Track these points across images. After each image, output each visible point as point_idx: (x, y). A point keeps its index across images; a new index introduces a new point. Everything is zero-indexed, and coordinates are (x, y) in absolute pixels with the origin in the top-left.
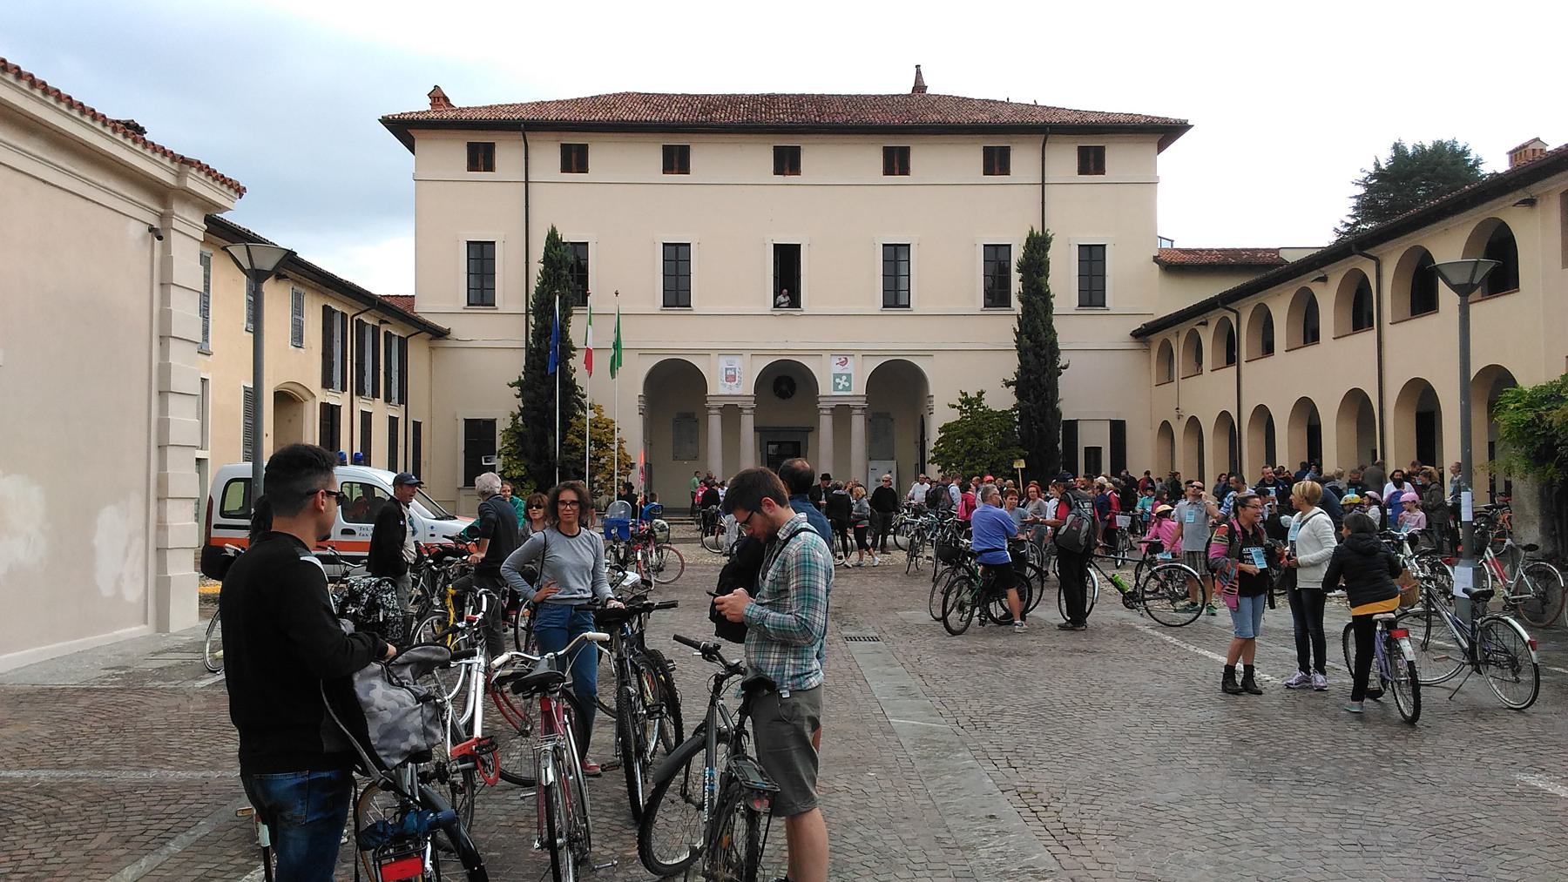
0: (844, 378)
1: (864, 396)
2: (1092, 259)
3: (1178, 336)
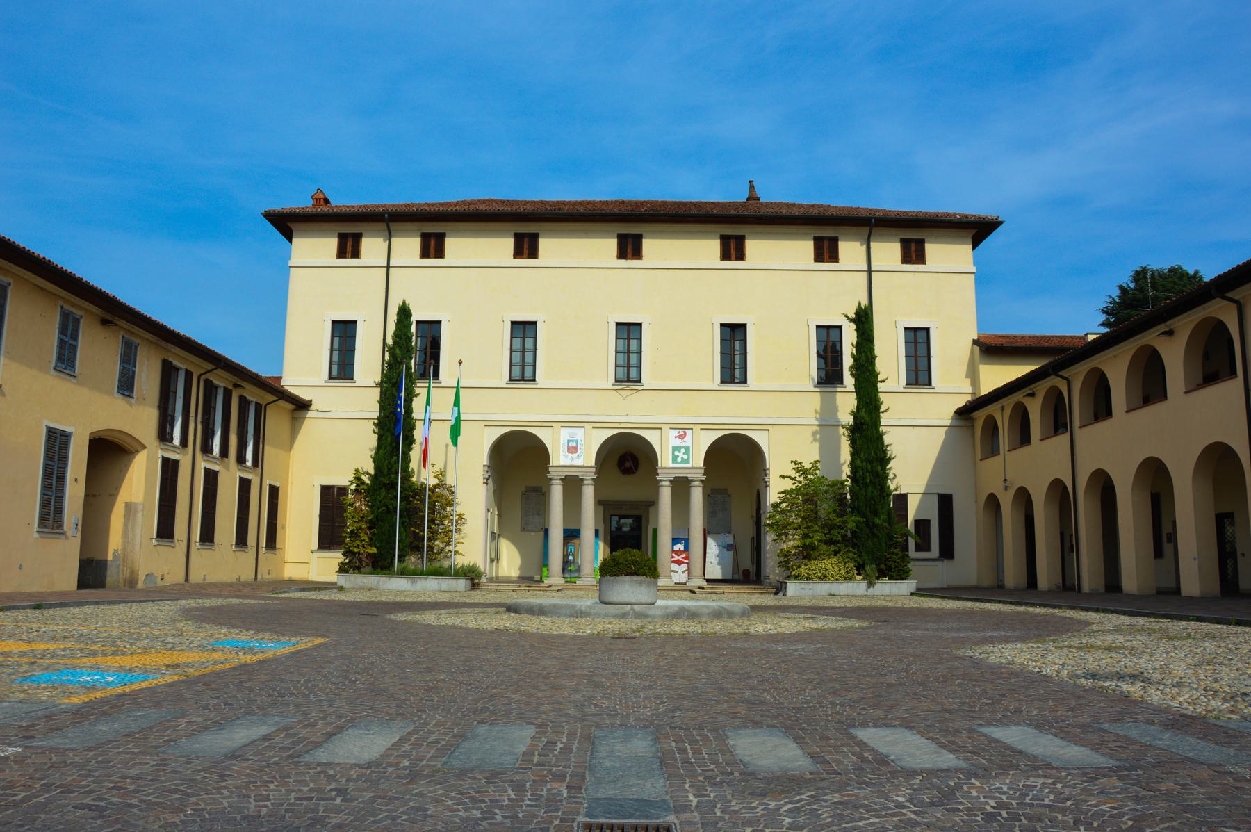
0: (683, 450)
1: (700, 468)
2: (918, 340)
3: (1003, 410)
